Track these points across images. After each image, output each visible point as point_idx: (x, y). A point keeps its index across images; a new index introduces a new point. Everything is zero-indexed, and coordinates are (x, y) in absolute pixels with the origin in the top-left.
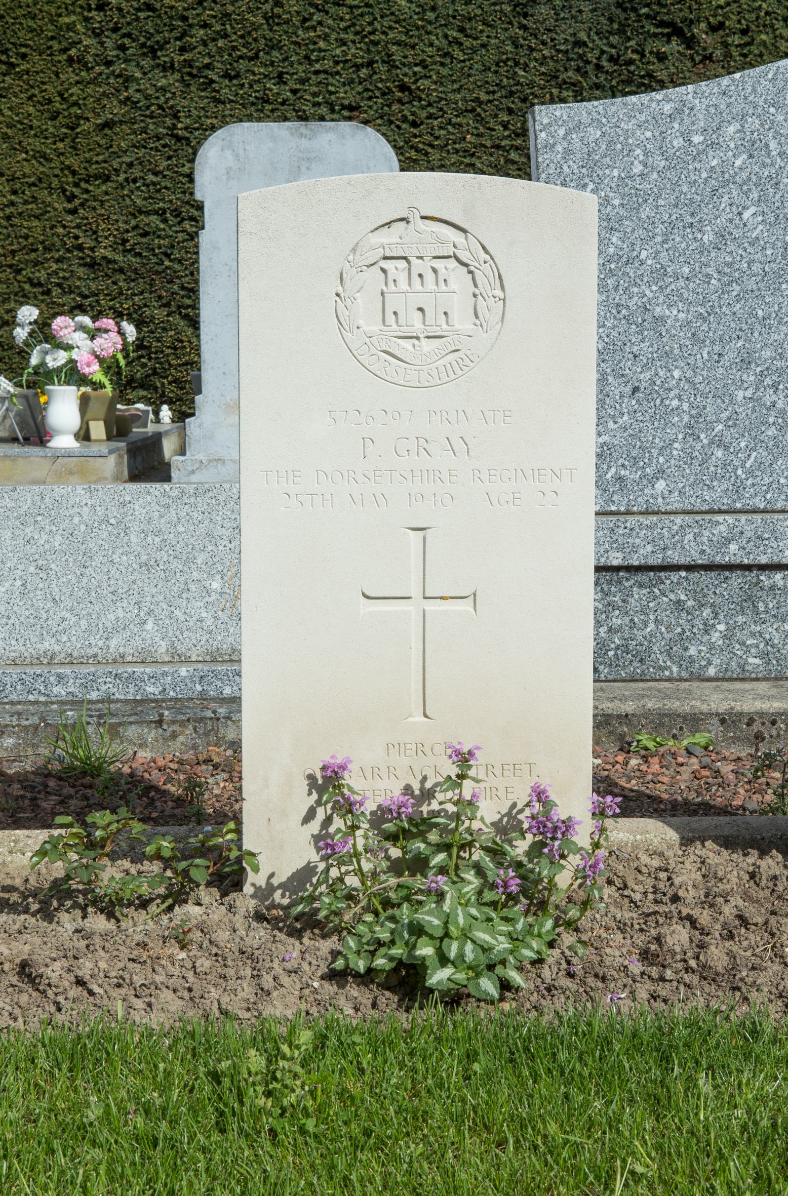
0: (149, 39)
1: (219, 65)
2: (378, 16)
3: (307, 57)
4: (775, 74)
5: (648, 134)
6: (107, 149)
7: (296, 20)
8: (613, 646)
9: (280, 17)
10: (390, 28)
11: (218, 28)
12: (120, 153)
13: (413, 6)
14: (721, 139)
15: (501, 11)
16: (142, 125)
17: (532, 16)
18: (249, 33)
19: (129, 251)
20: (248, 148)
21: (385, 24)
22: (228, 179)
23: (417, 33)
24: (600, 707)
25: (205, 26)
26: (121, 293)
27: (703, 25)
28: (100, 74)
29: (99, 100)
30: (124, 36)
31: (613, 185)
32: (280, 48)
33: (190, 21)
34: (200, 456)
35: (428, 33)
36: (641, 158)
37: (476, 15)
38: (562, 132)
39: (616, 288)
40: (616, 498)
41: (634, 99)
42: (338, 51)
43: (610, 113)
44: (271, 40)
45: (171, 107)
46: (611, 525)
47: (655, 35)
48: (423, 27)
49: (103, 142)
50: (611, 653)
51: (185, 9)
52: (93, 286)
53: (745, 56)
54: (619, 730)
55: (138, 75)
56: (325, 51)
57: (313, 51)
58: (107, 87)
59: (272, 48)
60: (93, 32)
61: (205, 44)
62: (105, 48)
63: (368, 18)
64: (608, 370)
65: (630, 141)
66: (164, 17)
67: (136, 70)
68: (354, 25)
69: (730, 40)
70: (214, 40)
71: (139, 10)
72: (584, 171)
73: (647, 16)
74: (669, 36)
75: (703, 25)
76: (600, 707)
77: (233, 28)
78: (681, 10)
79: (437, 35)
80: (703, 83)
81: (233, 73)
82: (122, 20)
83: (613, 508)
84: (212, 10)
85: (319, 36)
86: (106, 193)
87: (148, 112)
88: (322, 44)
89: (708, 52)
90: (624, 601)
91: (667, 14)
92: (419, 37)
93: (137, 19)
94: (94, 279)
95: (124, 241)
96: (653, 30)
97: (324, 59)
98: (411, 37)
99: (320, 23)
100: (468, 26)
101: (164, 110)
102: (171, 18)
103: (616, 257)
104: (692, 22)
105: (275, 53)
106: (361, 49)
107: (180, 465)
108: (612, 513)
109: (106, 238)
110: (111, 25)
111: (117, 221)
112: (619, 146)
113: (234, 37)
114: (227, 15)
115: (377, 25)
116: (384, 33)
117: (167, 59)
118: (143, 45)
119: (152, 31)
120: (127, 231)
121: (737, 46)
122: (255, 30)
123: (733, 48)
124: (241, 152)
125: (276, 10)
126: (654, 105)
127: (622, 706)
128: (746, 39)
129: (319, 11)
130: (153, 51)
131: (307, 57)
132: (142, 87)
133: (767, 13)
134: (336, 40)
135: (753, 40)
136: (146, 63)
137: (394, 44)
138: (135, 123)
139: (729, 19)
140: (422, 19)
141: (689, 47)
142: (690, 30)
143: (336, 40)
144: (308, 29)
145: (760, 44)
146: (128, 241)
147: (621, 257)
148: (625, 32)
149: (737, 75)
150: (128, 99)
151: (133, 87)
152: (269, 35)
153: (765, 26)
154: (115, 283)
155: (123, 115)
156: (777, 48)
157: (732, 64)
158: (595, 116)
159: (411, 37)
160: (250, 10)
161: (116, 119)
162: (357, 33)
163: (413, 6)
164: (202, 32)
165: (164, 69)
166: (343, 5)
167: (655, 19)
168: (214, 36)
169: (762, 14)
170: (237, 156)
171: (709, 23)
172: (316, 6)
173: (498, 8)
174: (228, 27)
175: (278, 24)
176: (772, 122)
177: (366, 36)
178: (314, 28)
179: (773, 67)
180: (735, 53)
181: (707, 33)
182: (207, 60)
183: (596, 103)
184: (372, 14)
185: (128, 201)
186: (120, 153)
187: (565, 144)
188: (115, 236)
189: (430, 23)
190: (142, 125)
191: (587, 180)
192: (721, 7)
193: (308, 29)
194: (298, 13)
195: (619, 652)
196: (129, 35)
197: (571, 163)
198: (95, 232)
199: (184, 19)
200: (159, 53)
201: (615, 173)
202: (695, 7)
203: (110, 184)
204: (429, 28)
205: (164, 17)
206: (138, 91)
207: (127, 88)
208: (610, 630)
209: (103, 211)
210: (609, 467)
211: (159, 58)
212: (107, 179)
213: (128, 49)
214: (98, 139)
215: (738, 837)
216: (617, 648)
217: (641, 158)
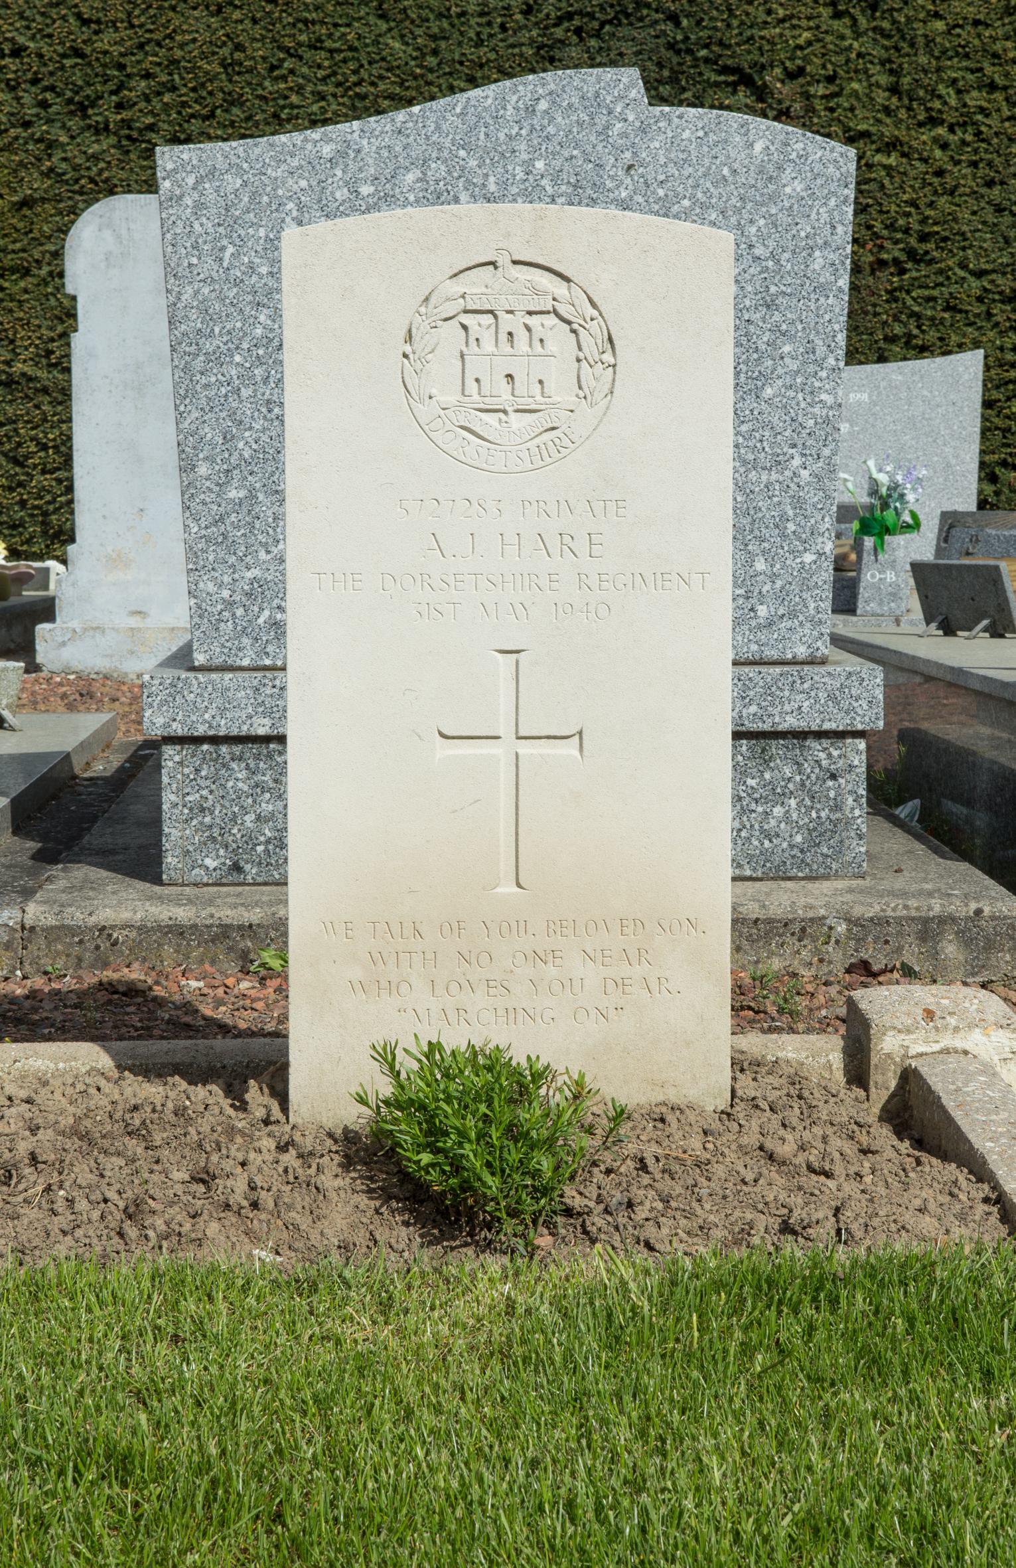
0: (77, 93)
1: (166, 127)
2: (365, 62)
3: (275, 116)
4: (465, 108)
5: (303, 183)
6: (26, 234)
7: (262, 68)
8: (262, 839)
9: (241, 64)
10: (381, 77)
11: (164, 78)
12: (43, 240)
13: (410, 50)
14: (397, 190)
15: (521, 55)
16: (70, 203)
17: (560, 60)
18: (203, 85)
19: (55, 365)
20: (132, 226)
21: (374, 72)
22: (108, 266)
23: (414, 84)
24: (217, 915)
25: (147, 76)
26: (45, 420)
27: (778, 71)
28: (16, 138)
29: (15, 171)
30: (46, 89)
31: (259, 248)
32: (242, 104)
33: (129, 70)
34: (75, 624)
35: (429, 83)
36: (295, 213)
37: (488, 61)
38: (191, 180)
39: (266, 380)
40: (270, 649)
41: (283, 138)
42: (315, 108)
43: (253, 157)
44: (230, 94)
45: (106, 181)
46: (255, 682)
47: (717, 84)
48: (422, 76)
49: (20, 225)
50: (260, 849)
51: (122, 55)
52: (10, 410)
53: (832, 110)
54: (242, 945)
55: (64, 139)
56: (298, 107)
57: (283, 107)
58: (24, 155)
59: (232, 103)
60: (7, 85)
61: (148, 100)
62: (22, 105)
63: (352, 65)
64: (258, 485)
65: (280, 192)
66: (96, 64)
67: (61, 132)
68: (335, 74)
69: (812, 90)
70: (159, 94)
71: (64, 56)
72: (221, 229)
73: (707, 60)
74: (734, 85)
75: (778, 71)
76: (217, 915)
77: (182, 78)
78: (749, 52)
79: (439, 86)
80: (372, 119)
81: (183, 137)
82: (43, 69)
83: (268, 662)
84: (156, 55)
85: (291, 89)
86: (26, 291)
87: (76, 187)
88: (294, 99)
89: (784, 106)
90: (276, 781)
91: (731, 57)
92: (418, 88)
93: (62, 68)
94: (11, 401)
95: (49, 353)
96: (714, 77)
97: (297, 118)
98: (408, 88)
99: (292, 71)
100: (479, 75)
101: (96, 184)
102: (105, 66)
103: (265, 341)
104: (763, 67)
105: (235, 110)
106: (343, 104)
107: (47, 636)
108: (266, 668)
109: (26, 349)
110: (29, 76)
111: (39, 327)
112: (265, 199)
113: (184, 90)
114: (174, 62)
115: (364, 74)
116: (373, 84)
117: (99, 119)
118: (70, 101)
119: (80, 83)
120: (52, 340)
121: (822, 97)
122: (210, 81)
123: (817, 101)
124: (124, 232)
125: (237, 55)
126: (309, 146)
127: (246, 914)
128: (833, 88)
129: (291, 56)
130: (82, 108)
131: (275, 116)
132: (69, 155)
133: (859, 55)
134: (313, 93)
135: (842, 89)
136: (74, 123)
137: (385, 98)
138: (60, 201)
139: (810, 62)
140: (421, 66)
141: (761, 99)
142: (762, 78)
143: (313, 93)
144: (277, 79)
145: (850, 95)
146: (53, 352)
147: (271, 340)
148: (678, 81)
149: (416, 109)
150: (51, 170)
151: (58, 155)
152: (229, 87)
153: (856, 71)
154: (37, 407)
155: (46, 191)
156: (872, 99)
157: (816, 120)
158: (234, 160)
159: (408, 88)
160: (204, 56)
161: (36, 196)
162: (339, 84)
163: (410, 50)
164: (143, 84)
165: (97, 132)
166: (321, 48)
167: (716, 63)
168: (158, 88)
169: (853, 56)
170: (119, 237)
171: (785, 69)
172: (287, 50)
173: (516, 51)
174: (176, 77)
175: (239, 73)
176: (463, 169)
177: (350, 88)
178: (284, 78)
179: (461, 98)
180: (819, 105)
181: (783, 82)
182: (149, 120)
183: (234, 144)
184: (358, 60)
185: (53, 302)
186: (43, 240)
187: (196, 195)
188: (37, 346)
189: (431, 70)
190: (70, 203)
191: (225, 242)
192: (800, 48)
193: (277, 79)
194: (264, 58)
195: (271, 847)
196: (52, 88)
197: (204, 220)
198: (12, 342)
199: (121, 67)
200: (90, 112)
201: (262, 232)
202: (767, 47)
203: (30, 279)
204: (430, 77)
205: (96, 64)
206: (64, 159)
207: (50, 156)
208: (258, 818)
209: (21, 315)
210: (261, 609)
211: (89, 117)
212: (27, 272)
213: (50, 106)
214: (14, 221)
215: (191, 1064)
216: (268, 842)
217: (295, 213)
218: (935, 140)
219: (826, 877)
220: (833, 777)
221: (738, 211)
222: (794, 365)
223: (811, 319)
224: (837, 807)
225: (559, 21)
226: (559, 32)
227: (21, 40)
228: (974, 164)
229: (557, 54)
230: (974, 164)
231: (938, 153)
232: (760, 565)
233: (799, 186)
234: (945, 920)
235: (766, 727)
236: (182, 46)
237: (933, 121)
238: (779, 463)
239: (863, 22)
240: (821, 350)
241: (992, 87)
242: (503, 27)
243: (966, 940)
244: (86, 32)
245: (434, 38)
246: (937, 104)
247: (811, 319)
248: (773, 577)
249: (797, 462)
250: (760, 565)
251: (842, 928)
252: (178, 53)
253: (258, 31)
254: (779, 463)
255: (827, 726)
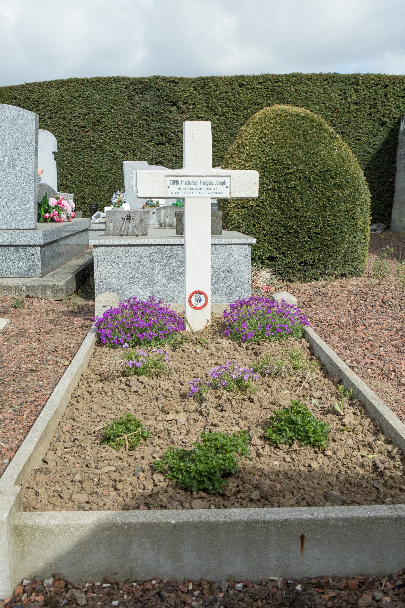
25: (43, 103)
74: (172, 105)
88: (75, 108)
160: (55, 99)
178: (73, 104)
182: (44, 114)
199: (38, 101)
218: (217, 119)
219: (32, 277)
220: (33, 255)
221: (9, 127)
222: (23, 162)
223: (26, 152)
224: (34, 262)
225: (133, 90)
226: (133, 93)
227: (16, 95)
228: (226, 124)
229: (133, 98)
230: (226, 124)
231: (217, 122)
232: (17, 208)
233: (22, 121)
234: (47, 286)
235: (17, 244)
236: (50, 96)
237: (216, 114)
238: (20, 184)
239: (201, 92)
240: (29, 159)
241: (229, 107)
242: (121, 92)
243: (52, 290)
244: (30, 94)
245: (106, 94)
246: (217, 110)
247: (26, 152)
248: (20, 210)
249: (25, 184)
250: (17, 208)
251: (24, 288)
252: (50, 98)
253: (67, 93)
254: (20, 184)
255: (30, 244)
